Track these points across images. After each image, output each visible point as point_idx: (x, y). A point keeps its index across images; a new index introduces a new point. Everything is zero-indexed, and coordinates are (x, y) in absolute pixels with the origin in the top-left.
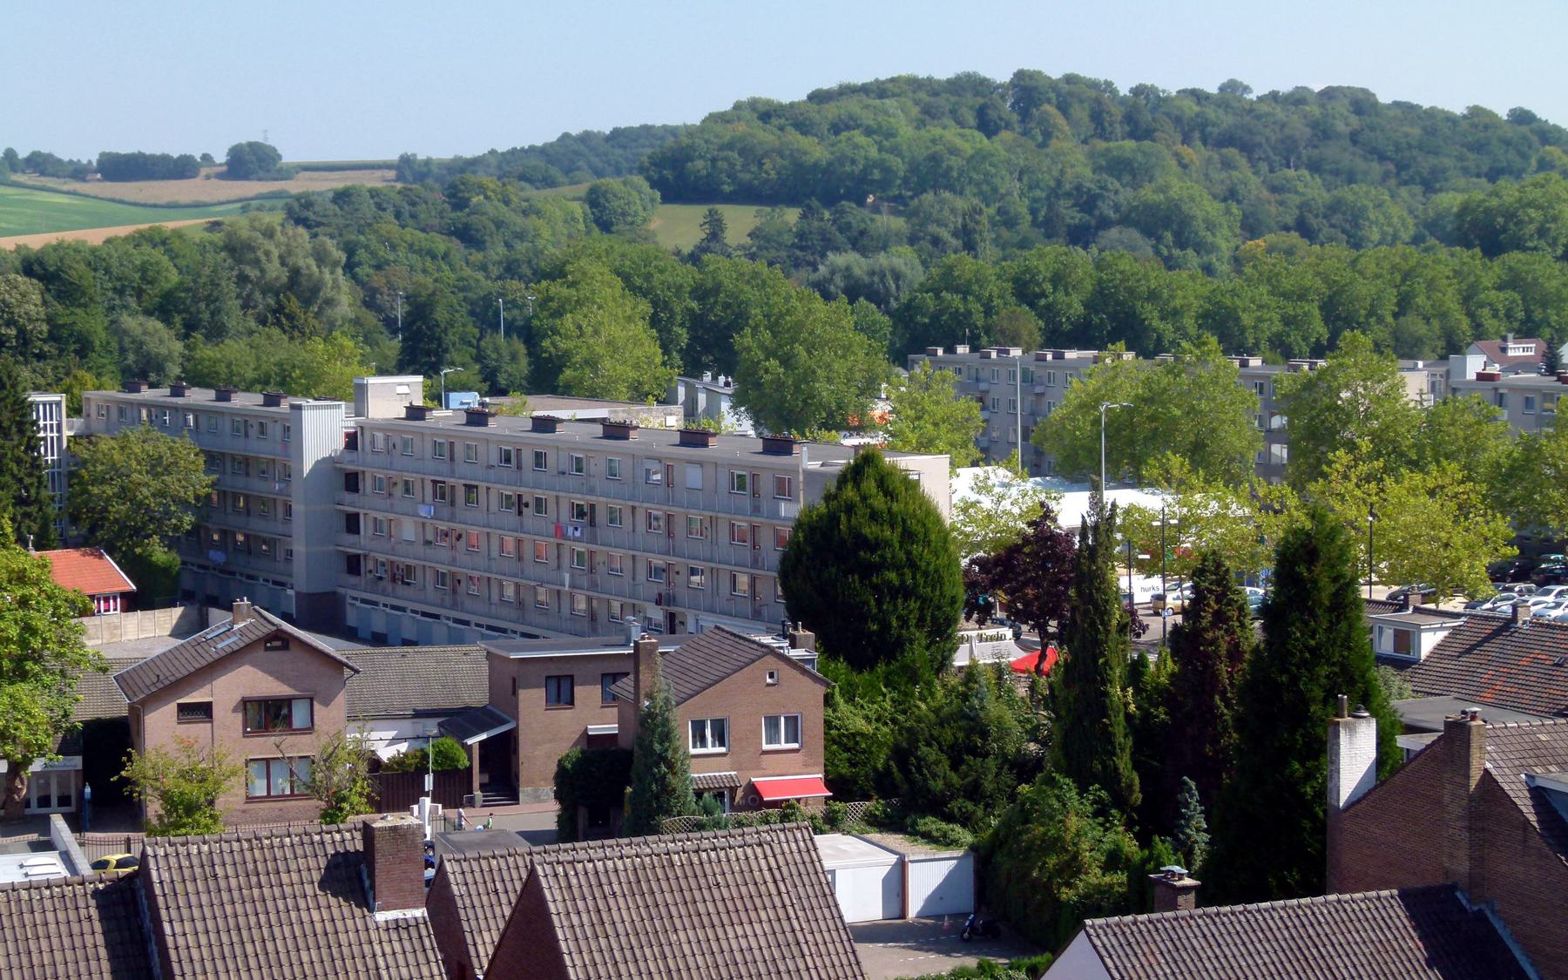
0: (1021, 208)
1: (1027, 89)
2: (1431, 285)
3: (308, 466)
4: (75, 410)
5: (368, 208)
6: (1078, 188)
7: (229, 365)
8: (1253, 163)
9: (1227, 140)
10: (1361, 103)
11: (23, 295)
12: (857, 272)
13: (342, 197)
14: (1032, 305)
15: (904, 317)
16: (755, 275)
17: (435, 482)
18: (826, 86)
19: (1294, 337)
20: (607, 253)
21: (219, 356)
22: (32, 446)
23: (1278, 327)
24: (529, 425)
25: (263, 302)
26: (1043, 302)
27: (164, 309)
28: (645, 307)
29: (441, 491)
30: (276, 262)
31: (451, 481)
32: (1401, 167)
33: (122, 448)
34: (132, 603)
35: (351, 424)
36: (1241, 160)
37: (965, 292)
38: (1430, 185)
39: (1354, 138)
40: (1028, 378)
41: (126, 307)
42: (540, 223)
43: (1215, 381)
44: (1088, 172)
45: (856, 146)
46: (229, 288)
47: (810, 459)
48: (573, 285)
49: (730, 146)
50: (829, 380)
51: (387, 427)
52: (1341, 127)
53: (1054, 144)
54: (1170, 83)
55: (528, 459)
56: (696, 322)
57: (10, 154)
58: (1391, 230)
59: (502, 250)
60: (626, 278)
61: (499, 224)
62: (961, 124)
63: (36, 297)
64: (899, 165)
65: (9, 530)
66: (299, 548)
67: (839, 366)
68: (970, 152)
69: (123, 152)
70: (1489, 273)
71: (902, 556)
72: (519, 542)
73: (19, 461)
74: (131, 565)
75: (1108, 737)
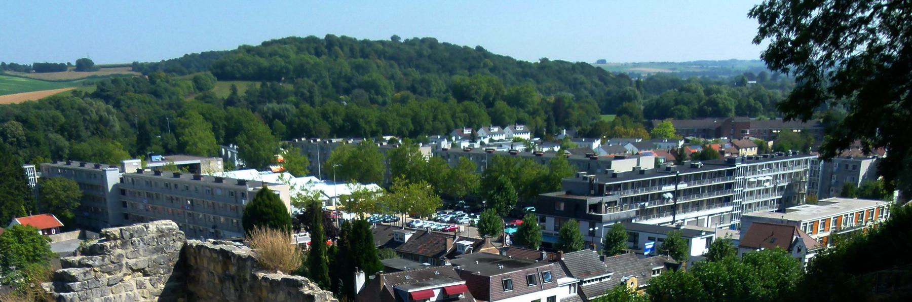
0: (328, 82)
2: (443, 113)
3: (110, 188)
4: (38, 169)
5: (124, 85)
6: (346, 75)
7: (83, 151)
8: (399, 65)
9: (392, 58)
11: (17, 128)
12: (276, 109)
14: (327, 121)
15: (289, 125)
16: (244, 113)
17: (147, 193)
18: (267, 40)
19: (404, 129)
20: (198, 107)
21: (80, 148)
23: (399, 125)
24: (172, 175)
25: (91, 127)
26: (330, 120)
27: (62, 130)
28: (210, 125)
29: (149, 196)
30: (95, 113)
31: (151, 192)
32: (443, 66)
33: (54, 183)
34: (61, 230)
36: (396, 65)
37: (307, 117)
38: (452, 72)
39: (429, 57)
40: (322, 149)
41: (49, 130)
43: (371, 151)
44: (349, 70)
45: (277, 61)
46: (80, 122)
47: (249, 187)
48: (187, 118)
49: (238, 61)
50: (264, 150)
51: (132, 176)
52: (425, 53)
53: (339, 60)
54: (373, 38)
55: (173, 185)
56: (226, 128)
57: (3, 64)
58: (439, 88)
59: (168, 99)
60: (203, 115)
61: (166, 90)
62: (310, 53)
63: (21, 128)
64: (291, 67)
65: (24, 209)
66: (110, 212)
67: (267, 146)
68: (313, 63)
69: (41, 62)
71: (274, 217)
72: (173, 211)
73: (24, 187)
75: (322, 268)
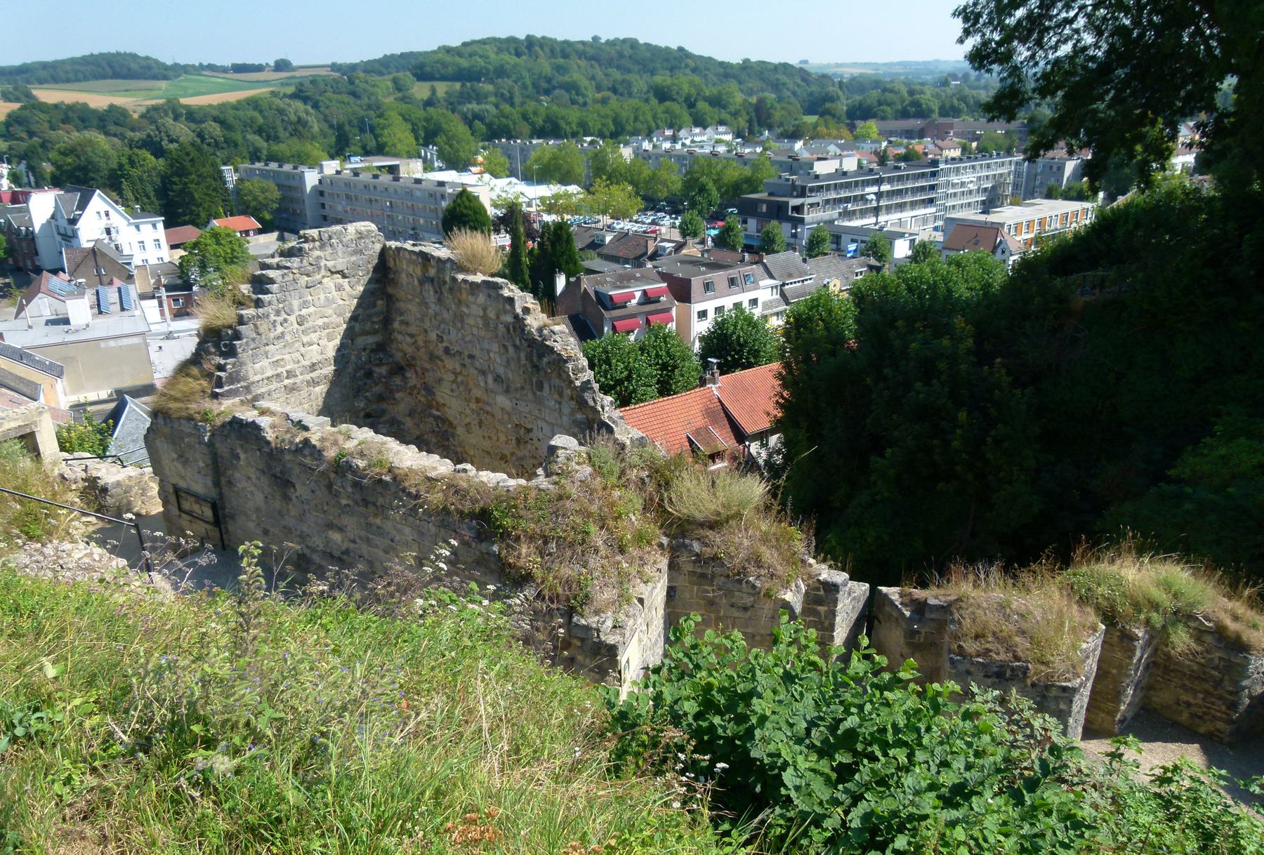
0: (528, 82)
1: (531, 42)
2: (644, 113)
3: (308, 189)
4: (236, 170)
5: (322, 86)
8: (600, 66)
10: (633, 44)
13: (313, 82)
19: (605, 130)
22: (225, 183)
27: (259, 131)
29: (348, 197)
32: (644, 67)
35: (319, 176)
36: (596, 65)
37: (507, 118)
38: (653, 73)
39: (630, 57)
40: (522, 150)
42: (378, 90)
46: (278, 123)
48: (386, 119)
52: (626, 53)
55: (372, 187)
59: (366, 100)
60: (403, 116)
61: (365, 90)
62: (510, 54)
63: (219, 129)
64: (491, 68)
66: (309, 214)
70: (660, 109)
74: (260, 220)
